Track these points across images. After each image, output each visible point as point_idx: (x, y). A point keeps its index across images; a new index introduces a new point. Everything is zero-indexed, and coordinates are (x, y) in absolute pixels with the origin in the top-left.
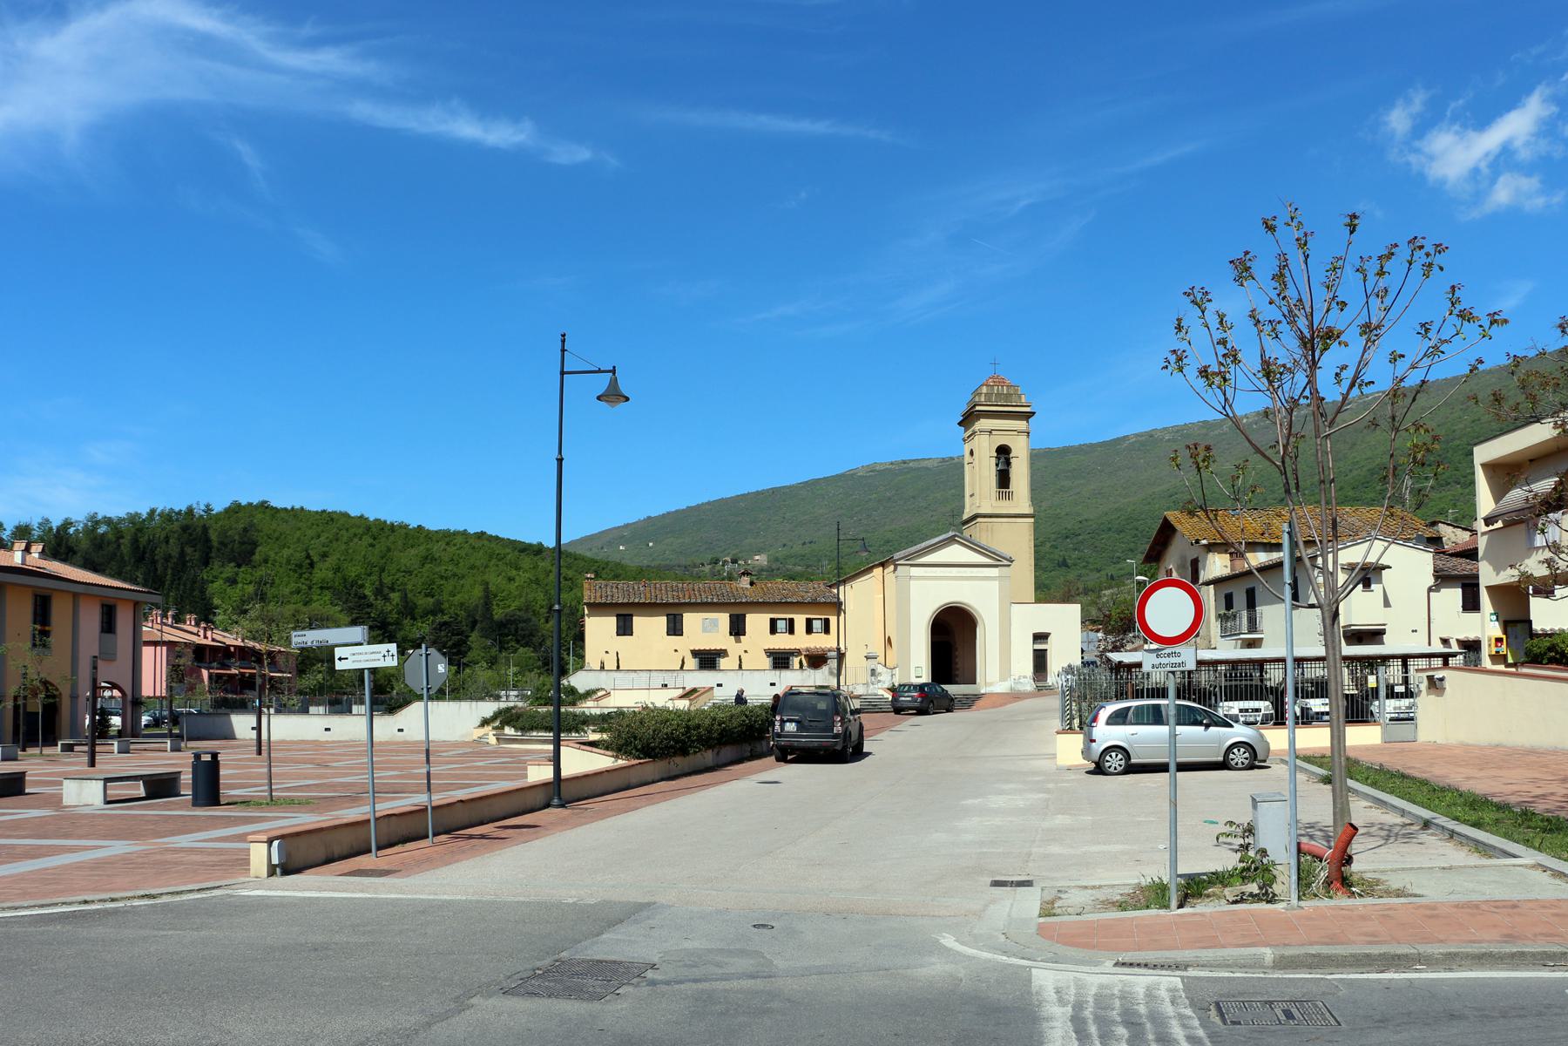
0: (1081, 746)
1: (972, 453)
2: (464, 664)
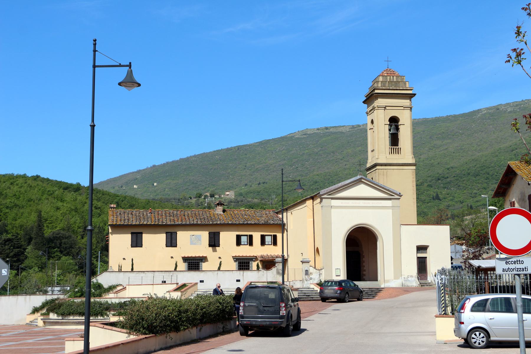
0: (453, 326)
1: (372, 122)
2: (22, 269)
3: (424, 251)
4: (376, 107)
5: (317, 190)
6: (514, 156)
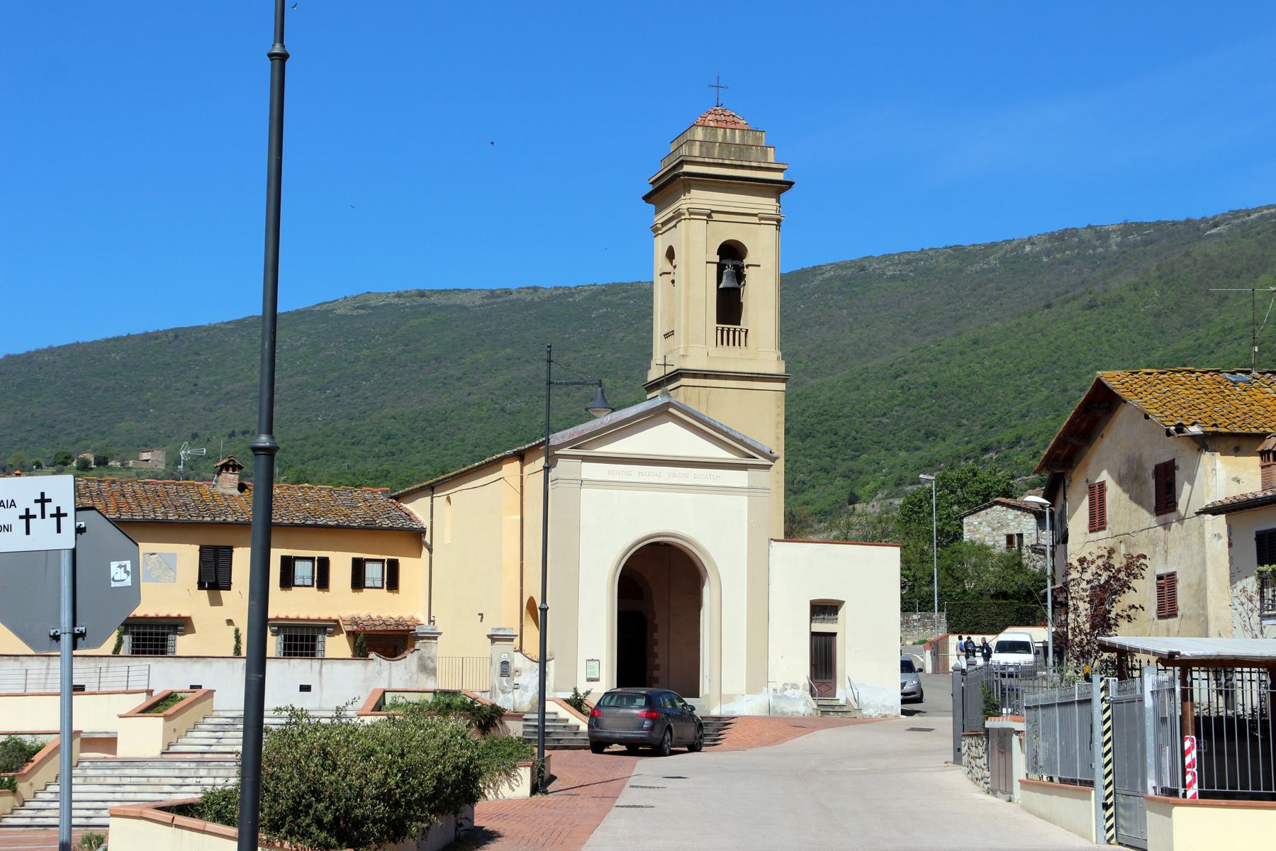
1: (670, 254)
3: (829, 617)
5: (391, 458)
6: (901, 391)
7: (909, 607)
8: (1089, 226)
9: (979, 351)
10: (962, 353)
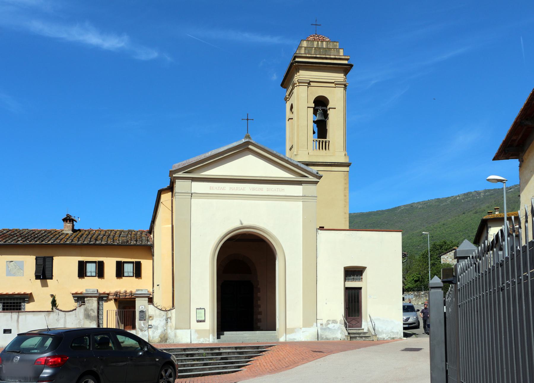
3: (357, 277)
4: (297, 82)
7: (420, 289)
8: (475, 191)
9: (444, 227)
10: (440, 228)
